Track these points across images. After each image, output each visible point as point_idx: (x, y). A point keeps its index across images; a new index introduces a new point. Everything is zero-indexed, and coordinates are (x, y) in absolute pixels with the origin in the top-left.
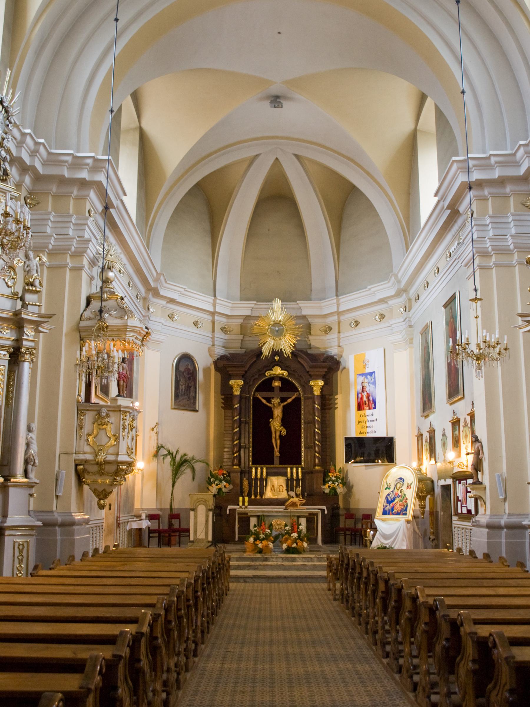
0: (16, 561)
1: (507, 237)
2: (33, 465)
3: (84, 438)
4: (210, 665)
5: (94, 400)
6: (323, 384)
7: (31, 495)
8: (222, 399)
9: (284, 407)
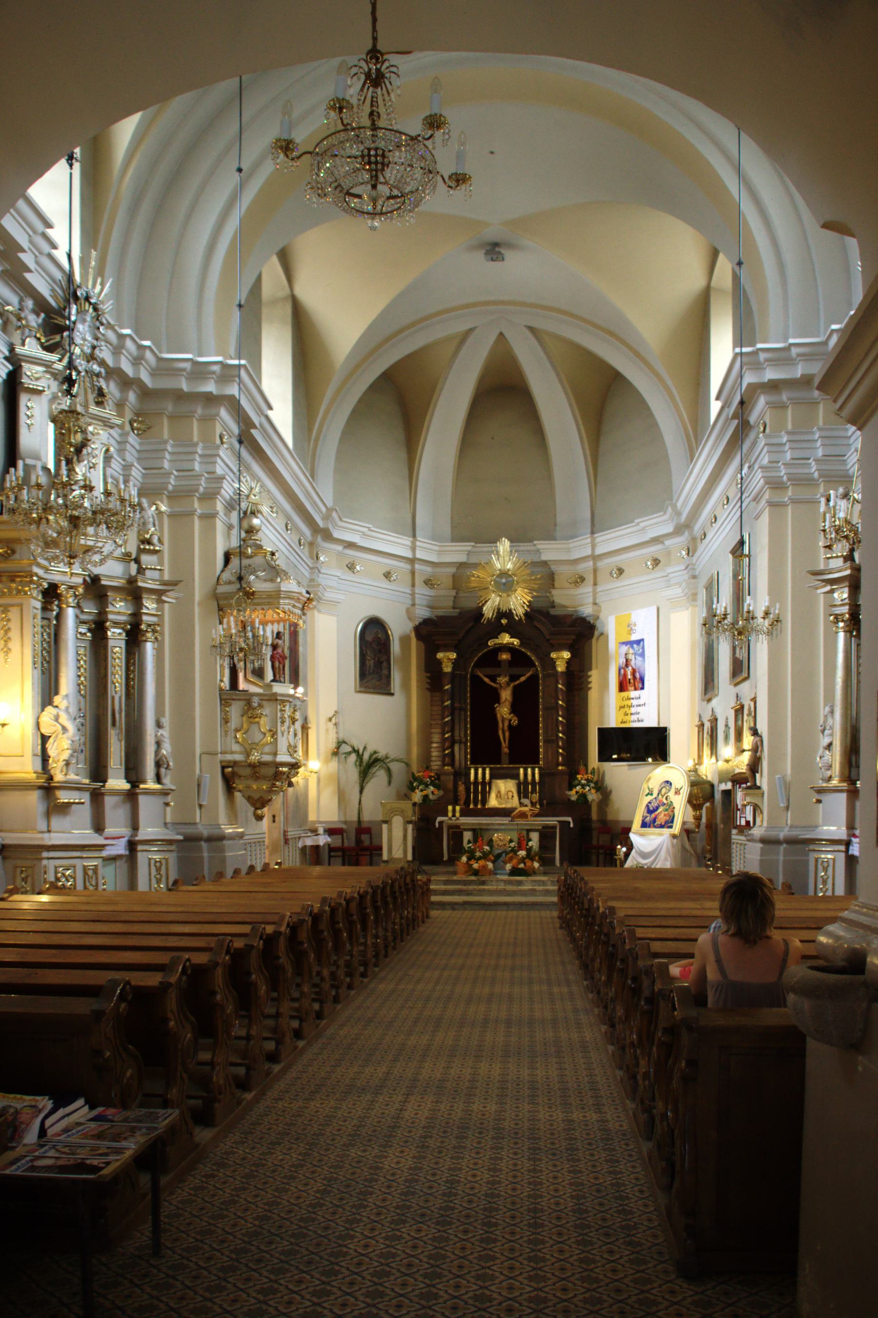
0: (154, 881)
1: (810, 461)
2: (166, 768)
4: (381, 987)
5: (242, 685)
6: (569, 656)
7: (167, 804)
8: (427, 677)
9: (515, 687)
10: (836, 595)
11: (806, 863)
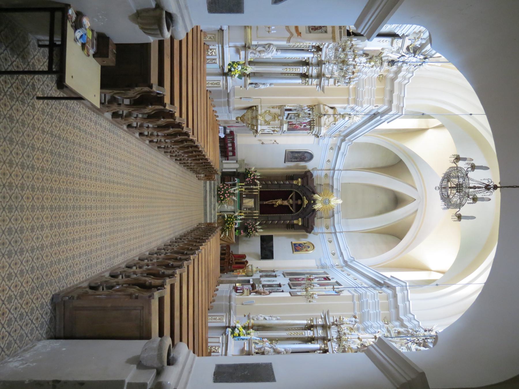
0: (212, 82)
3: (268, 109)
10: (320, 320)
11: (222, 312)
